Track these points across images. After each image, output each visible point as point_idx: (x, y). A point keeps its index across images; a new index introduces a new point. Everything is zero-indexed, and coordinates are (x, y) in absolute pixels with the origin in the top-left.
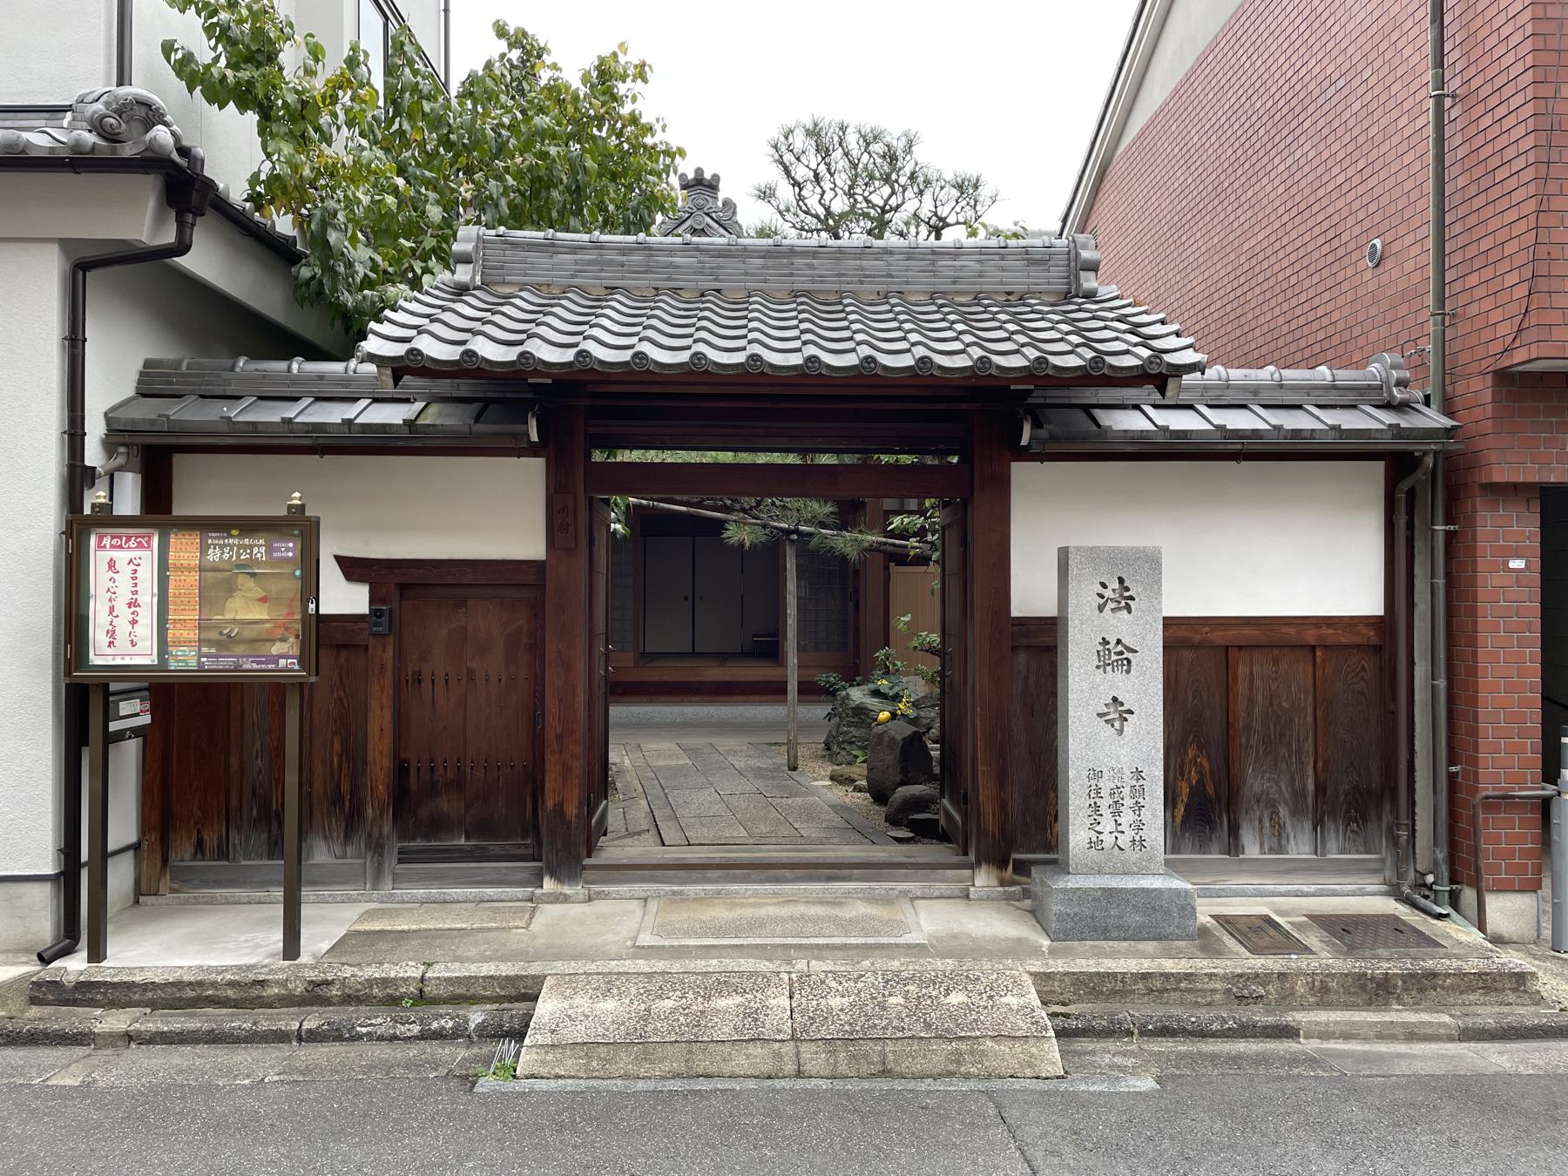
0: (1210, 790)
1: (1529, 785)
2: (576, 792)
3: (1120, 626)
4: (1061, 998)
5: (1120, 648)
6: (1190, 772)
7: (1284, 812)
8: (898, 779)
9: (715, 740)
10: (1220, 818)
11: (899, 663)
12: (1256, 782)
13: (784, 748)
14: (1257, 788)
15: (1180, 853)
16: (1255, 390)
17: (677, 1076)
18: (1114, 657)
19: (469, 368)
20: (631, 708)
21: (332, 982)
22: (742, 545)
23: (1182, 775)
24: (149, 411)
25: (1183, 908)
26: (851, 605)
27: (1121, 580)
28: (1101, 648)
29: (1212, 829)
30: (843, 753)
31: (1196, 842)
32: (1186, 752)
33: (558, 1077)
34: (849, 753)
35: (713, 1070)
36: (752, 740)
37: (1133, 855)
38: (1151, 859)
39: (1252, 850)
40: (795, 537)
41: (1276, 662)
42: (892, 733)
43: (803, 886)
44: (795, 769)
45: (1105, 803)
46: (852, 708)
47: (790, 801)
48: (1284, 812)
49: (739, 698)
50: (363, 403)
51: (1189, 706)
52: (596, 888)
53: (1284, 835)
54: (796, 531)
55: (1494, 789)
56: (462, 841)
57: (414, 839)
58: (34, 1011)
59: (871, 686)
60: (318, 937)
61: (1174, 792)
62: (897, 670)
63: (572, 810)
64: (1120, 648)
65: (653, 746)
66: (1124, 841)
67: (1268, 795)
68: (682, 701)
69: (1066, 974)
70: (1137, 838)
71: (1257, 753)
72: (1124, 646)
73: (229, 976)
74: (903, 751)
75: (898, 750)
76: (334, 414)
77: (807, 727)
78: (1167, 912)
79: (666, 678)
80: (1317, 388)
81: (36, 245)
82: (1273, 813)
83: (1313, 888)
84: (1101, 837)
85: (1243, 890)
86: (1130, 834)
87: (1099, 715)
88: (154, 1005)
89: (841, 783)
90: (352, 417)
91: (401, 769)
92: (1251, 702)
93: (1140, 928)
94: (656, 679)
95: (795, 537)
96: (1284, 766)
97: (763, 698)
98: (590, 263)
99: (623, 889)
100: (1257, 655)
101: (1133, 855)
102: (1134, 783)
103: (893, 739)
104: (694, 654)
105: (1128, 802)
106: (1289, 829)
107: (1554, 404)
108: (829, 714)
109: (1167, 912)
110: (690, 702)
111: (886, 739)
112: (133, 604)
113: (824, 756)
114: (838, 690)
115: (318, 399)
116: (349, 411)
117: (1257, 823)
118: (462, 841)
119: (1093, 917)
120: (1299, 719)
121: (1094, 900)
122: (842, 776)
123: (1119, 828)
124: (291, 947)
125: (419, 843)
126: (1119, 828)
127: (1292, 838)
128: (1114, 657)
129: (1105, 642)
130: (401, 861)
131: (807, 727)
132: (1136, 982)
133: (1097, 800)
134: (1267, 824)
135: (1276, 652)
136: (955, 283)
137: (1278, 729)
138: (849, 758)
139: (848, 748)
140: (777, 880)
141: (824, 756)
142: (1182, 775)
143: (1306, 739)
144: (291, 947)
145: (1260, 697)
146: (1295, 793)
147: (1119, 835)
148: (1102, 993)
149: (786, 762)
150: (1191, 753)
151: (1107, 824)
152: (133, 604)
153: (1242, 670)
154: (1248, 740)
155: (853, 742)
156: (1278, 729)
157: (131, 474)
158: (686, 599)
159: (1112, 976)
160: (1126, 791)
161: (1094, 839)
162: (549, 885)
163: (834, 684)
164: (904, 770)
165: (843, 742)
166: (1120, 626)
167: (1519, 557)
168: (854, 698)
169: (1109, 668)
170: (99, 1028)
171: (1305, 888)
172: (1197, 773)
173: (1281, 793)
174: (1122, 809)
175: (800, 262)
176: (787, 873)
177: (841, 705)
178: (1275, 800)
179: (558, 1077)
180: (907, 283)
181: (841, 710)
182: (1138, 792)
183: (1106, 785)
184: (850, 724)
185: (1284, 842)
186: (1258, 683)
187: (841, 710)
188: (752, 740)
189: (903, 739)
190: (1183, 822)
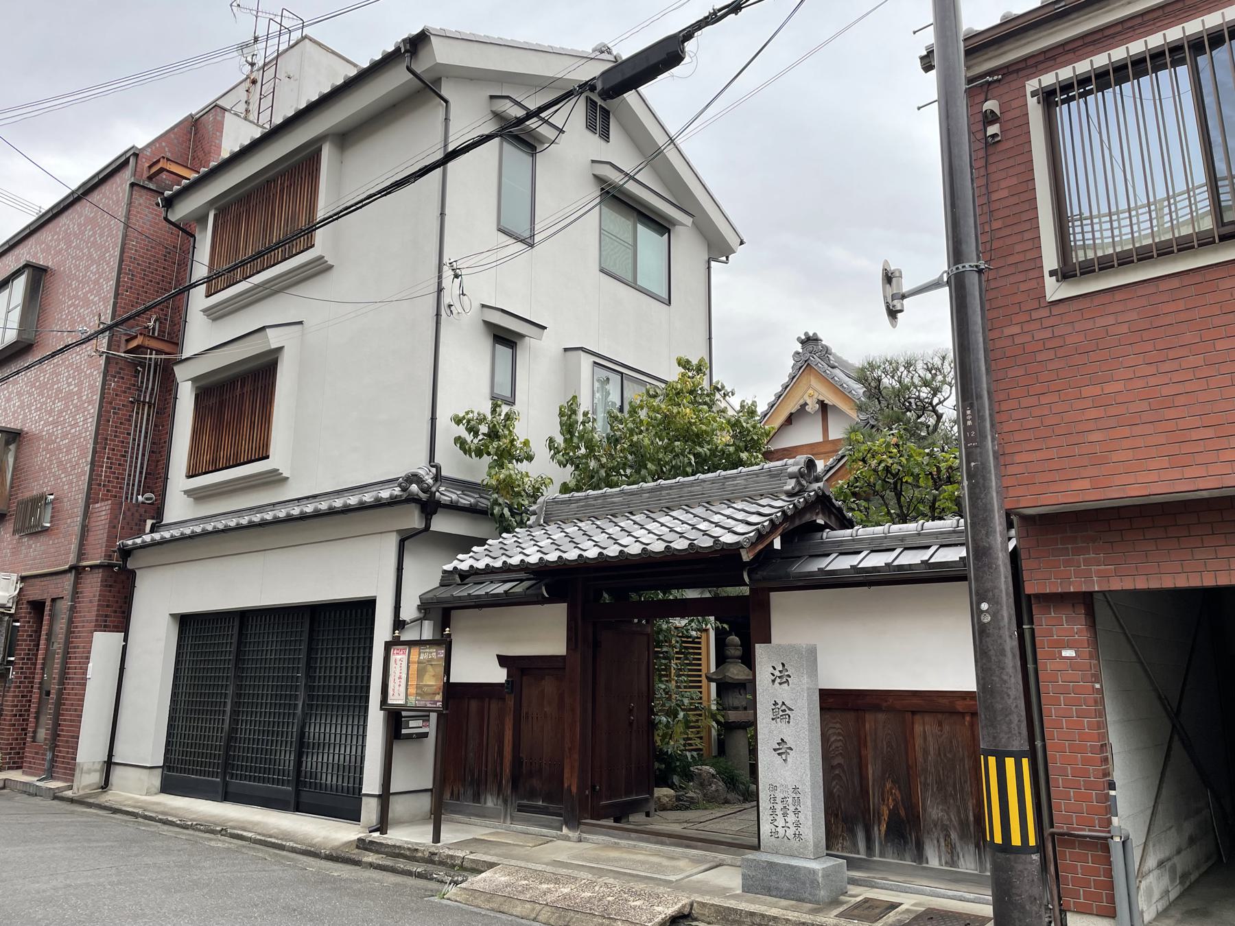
0: (902, 813)
1: (1098, 828)
2: (576, 780)
3: (784, 693)
4: (708, 920)
5: (784, 707)
6: (888, 800)
7: (954, 836)
10: (911, 835)
12: (934, 811)
14: (934, 816)
15: (885, 857)
16: (902, 538)
17: (493, 910)
18: (781, 713)
19: (524, 567)
21: (436, 854)
23: (883, 800)
24: (445, 593)
25: (812, 882)
27: (783, 664)
28: (774, 707)
29: (906, 843)
31: (895, 851)
32: (884, 784)
33: (456, 901)
35: (506, 910)
37: (795, 844)
38: (805, 847)
39: (934, 862)
41: (940, 724)
43: (673, 848)
45: (779, 807)
48: (954, 836)
50: (933, 549)
51: (885, 752)
52: (584, 835)
53: (955, 854)
55: (1090, 830)
56: (541, 803)
57: (523, 800)
58: (356, 851)
60: (448, 836)
61: (878, 813)
63: (574, 790)
64: (784, 707)
66: (790, 833)
67: (942, 822)
69: (713, 905)
70: (797, 833)
71: (932, 790)
72: (787, 707)
73: (409, 846)
76: (877, 560)
78: (804, 883)
80: (942, 533)
81: (242, 555)
82: (946, 835)
83: (972, 896)
84: (778, 829)
85: (922, 890)
86: (793, 829)
87: (775, 750)
88: (388, 854)
90: (856, 564)
91: (517, 761)
92: (926, 752)
93: (789, 891)
96: (952, 801)
98: (582, 506)
99: (594, 837)
100: (927, 718)
101: (795, 844)
102: (794, 795)
105: (792, 808)
106: (959, 849)
107: (1068, 534)
109: (804, 883)
112: (400, 678)
115: (841, 554)
116: (923, 555)
117: (936, 842)
118: (541, 803)
119: (763, 880)
120: (960, 766)
121: (763, 868)
123: (787, 825)
124: (436, 838)
125: (525, 802)
126: (787, 825)
127: (961, 856)
128: (781, 713)
129: (776, 704)
130: (518, 811)
132: (746, 917)
133: (775, 805)
134: (942, 841)
135: (940, 716)
136: (732, 493)
137: (946, 773)
140: (662, 843)
142: (883, 800)
143: (965, 782)
144: (436, 838)
145: (931, 749)
146: (961, 823)
147: (787, 829)
148: (728, 920)
150: (888, 785)
151: (780, 822)
152: (400, 678)
153: (918, 729)
154: (926, 778)
156: (946, 773)
157: (427, 621)
159: (735, 911)
160: (790, 800)
161: (774, 831)
162: (565, 830)
166: (784, 693)
167: (1071, 648)
169: (778, 720)
170: (365, 859)
171: (967, 895)
172: (893, 800)
173: (951, 820)
174: (788, 812)
175: (664, 492)
176: (666, 839)
178: (947, 825)
179: (456, 901)
180: (710, 496)
182: (797, 801)
183: (779, 796)
185: (955, 858)
186: (930, 739)
190: (885, 834)
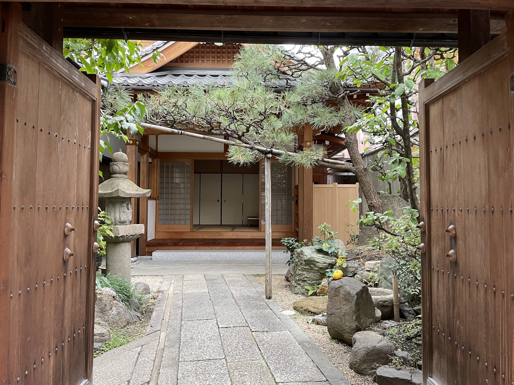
8: (354, 325)
9: (225, 272)
11: (332, 233)
13: (263, 279)
20: (185, 253)
22: (239, 164)
26: (293, 203)
30: (299, 287)
34: (303, 287)
36: (245, 273)
40: (270, 156)
42: (348, 288)
44: (270, 298)
46: (305, 261)
47: (270, 335)
49: (239, 247)
54: (271, 152)
59: (317, 247)
62: (332, 237)
65: (190, 277)
68: (212, 249)
74: (357, 304)
75: (354, 303)
77: (275, 263)
79: (205, 237)
89: (302, 313)
94: (201, 237)
95: (270, 156)
97: (252, 247)
103: (349, 293)
104: (221, 226)
108: (288, 261)
110: (216, 249)
111: (342, 291)
113: (286, 286)
114: (295, 248)
122: (302, 308)
131: (275, 263)
138: (303, 291)
139: (302, 284)
141: (286, 286)
149: (263, 290)
155: (306, 281)
158: (218, 201)
163: (293, 244)
164: (358, 318)
165: (299, 280)
168: (306, 254)
177: (297, 257)
181: (297, 260)
184: (304, 270)
187: (297, 260)
188: (245, 273)
189: (357, 294)
